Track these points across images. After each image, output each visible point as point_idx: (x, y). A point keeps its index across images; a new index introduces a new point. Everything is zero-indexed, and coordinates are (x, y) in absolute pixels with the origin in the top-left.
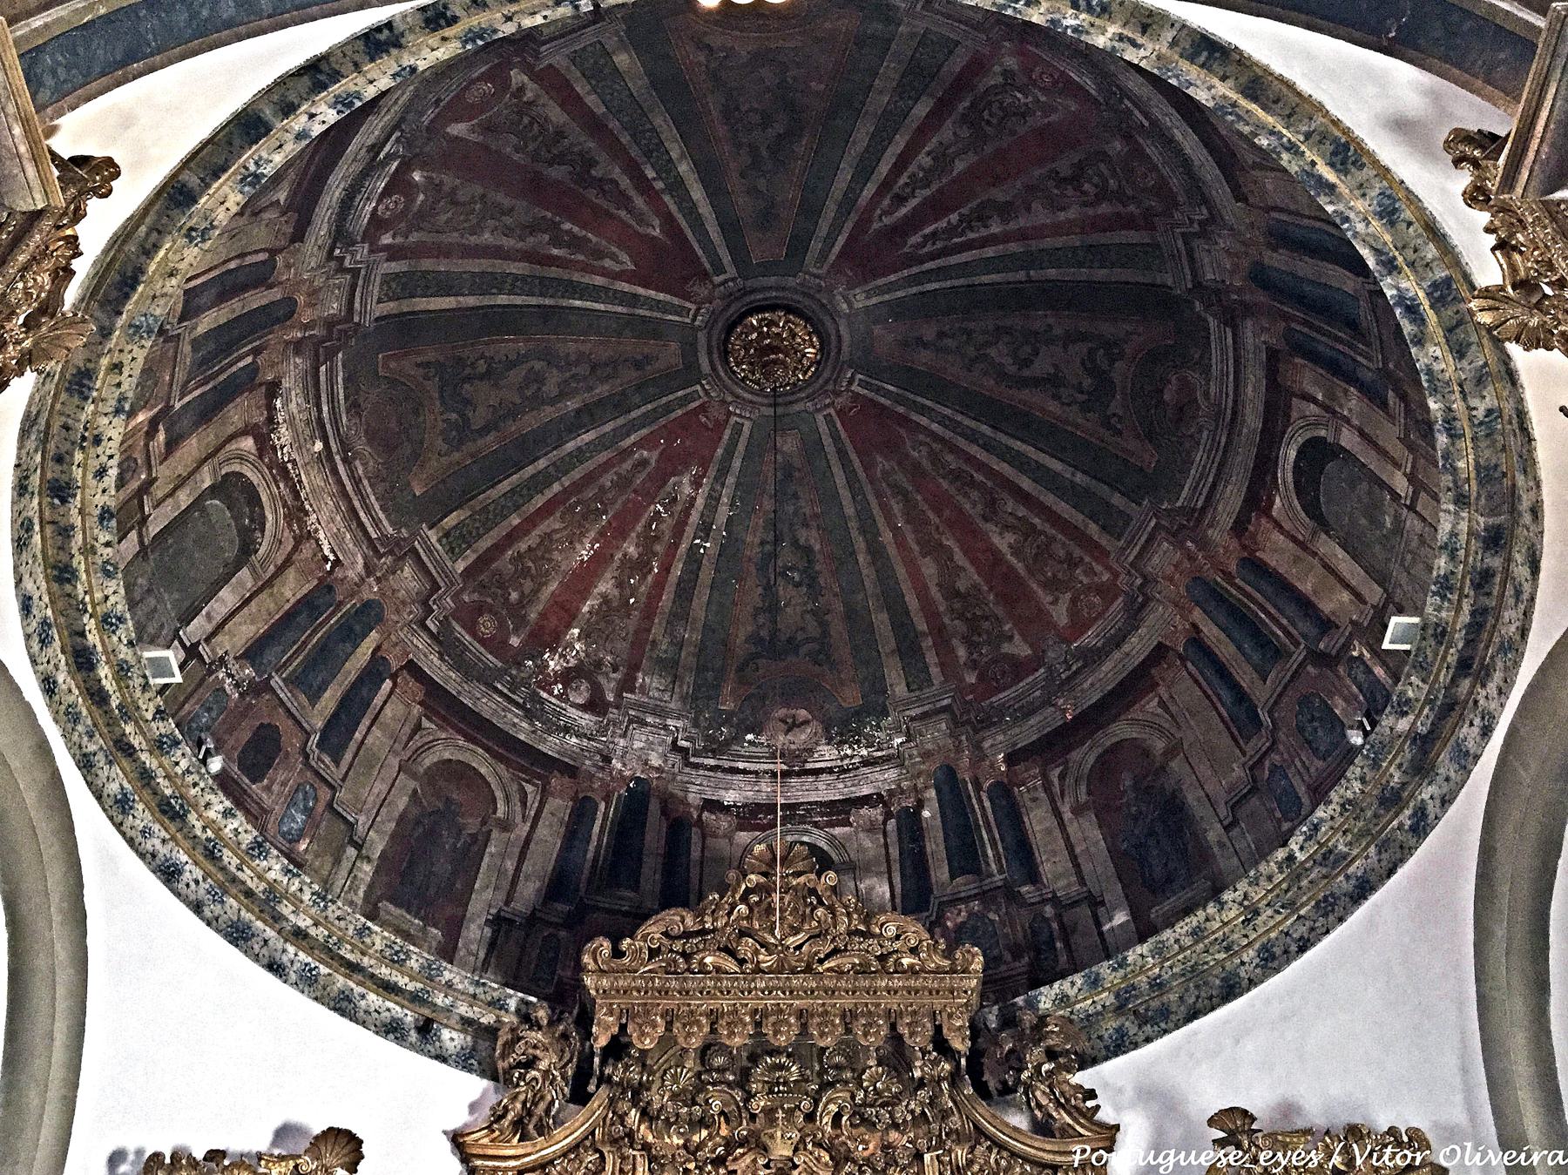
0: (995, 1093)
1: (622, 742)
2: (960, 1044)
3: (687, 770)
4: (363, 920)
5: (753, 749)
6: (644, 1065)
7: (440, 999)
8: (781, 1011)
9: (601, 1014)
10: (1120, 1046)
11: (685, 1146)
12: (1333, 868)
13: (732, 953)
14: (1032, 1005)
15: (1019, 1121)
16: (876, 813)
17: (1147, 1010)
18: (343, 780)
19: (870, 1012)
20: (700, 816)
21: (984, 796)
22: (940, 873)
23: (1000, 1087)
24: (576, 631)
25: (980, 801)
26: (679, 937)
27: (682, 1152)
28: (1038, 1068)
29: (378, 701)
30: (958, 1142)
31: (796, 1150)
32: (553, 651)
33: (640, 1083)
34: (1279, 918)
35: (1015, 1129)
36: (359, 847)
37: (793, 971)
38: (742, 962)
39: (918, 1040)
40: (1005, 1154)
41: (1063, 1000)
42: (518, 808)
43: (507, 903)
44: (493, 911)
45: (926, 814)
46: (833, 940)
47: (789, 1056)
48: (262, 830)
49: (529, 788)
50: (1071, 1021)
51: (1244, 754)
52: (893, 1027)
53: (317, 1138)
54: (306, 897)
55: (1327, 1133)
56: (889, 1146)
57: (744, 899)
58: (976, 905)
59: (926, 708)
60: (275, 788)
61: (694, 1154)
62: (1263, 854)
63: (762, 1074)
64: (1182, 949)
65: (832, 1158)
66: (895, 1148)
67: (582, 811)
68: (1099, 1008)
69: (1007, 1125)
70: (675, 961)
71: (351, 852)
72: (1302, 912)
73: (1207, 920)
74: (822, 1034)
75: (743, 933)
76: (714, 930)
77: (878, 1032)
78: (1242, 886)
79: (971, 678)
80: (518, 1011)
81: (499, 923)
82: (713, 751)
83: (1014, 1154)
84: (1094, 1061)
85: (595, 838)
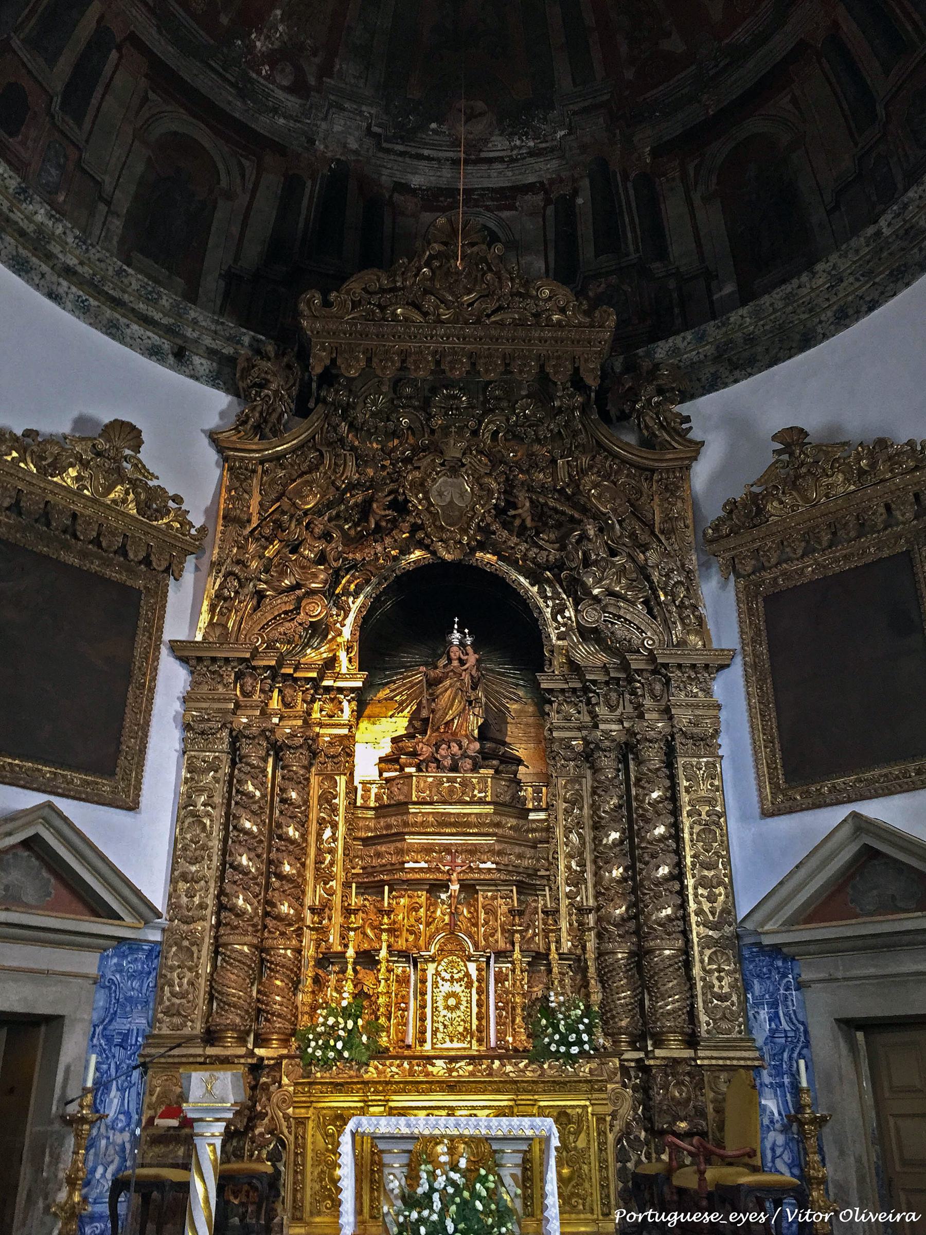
0: (614, 418)
1: (324, 125)
2: (593, 382)
3: (381, 155)
4: (119, 263)
5: (437, 137)
6: (350, 391)
7: (189, 333)
8: (456, 353)
9: (316, 350)
10: (714, 385)
11: (382, 449)
12: (911, 242)
13: (418, 307)
14: (649, 354)
15: (631, 439)
16: (537, 199)
17: (738, 359)
18: (87, 141)
19: (525, 355)
20: (391, 197)
21: (630, 185)
22: (587, 251)
23: (618, 414)
24: (278, 12)
25: (626, 189)
26: (376, 293)
27: (380, 453)
28: (649, 401)
29: (108, 69)
30: (584, 453)
31: (464, 454)
32: (259, 32)
33: (348, 403)
34: (857, 284)
35: (627, 444)
36: (108, 203)
37: (466, 323)
38: (425, 314)
39: (561, 378)
40: (617, 461)
41: (676, 351)
42: (238, 181)
43: (236, 260)
44: (225, 267)
45: (580, 201)
46: (499, 300)
47: (460, 389)
48: (24, 179)
49: (247, 163)
50: (679, 368)
51: (856, 144)
52: (542, 367)
53: (106, 426)
54: (70, 240)
55: (861, 444)
56: (533, 454)
57: (427, 264)
58: (614, 279)
59: (586, 104)
60: (30, 143)
61: (389, 455)
62: (855, 231)
63: (440, 402)
64: (775, 311)
65: (490, 461)
66: (537, 456)
67: (292, 186)
68: (702, 356)
69: (621, 441)
70: (373, 312)
71: (102, 208)
72: (877, 280)
73: (800, 287)
74: (487, 371)
75: (426, 292)
76: (403, 289)
77: (530, 370)
78: (834, 258)
79: (629, 74)
80: (251, 345)
81: (231, 278)
82: (402, 138)
83: (624, 461)
84: (693, 397)
85: (304, 212)
